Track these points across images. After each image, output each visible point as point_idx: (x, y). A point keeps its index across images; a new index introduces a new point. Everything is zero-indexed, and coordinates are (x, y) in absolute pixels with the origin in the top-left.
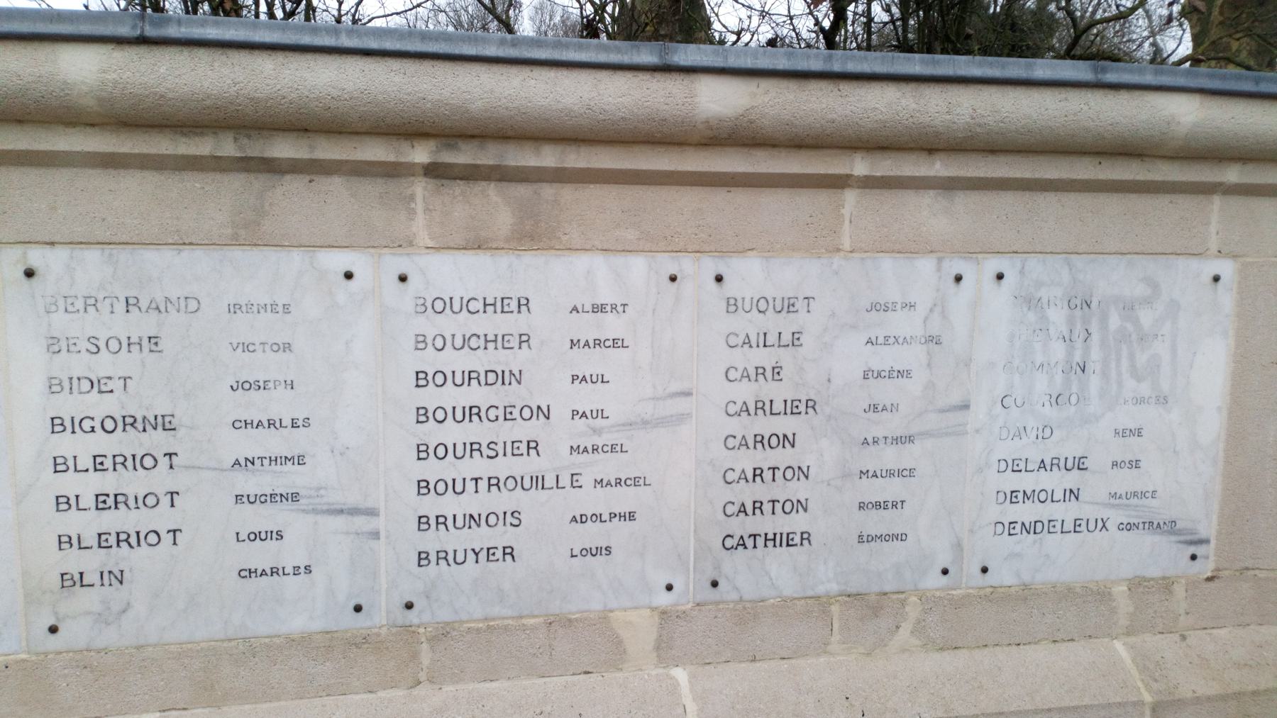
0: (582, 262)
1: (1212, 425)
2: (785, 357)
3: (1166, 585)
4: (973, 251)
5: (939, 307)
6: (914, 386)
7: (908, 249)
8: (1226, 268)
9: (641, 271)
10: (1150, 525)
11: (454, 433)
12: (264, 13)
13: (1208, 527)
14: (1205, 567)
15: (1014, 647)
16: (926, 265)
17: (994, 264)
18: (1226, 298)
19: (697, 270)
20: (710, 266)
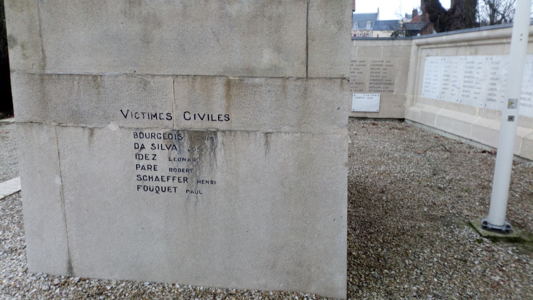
9: (484, 57)
11: (468, 84)
19: (489, 57)
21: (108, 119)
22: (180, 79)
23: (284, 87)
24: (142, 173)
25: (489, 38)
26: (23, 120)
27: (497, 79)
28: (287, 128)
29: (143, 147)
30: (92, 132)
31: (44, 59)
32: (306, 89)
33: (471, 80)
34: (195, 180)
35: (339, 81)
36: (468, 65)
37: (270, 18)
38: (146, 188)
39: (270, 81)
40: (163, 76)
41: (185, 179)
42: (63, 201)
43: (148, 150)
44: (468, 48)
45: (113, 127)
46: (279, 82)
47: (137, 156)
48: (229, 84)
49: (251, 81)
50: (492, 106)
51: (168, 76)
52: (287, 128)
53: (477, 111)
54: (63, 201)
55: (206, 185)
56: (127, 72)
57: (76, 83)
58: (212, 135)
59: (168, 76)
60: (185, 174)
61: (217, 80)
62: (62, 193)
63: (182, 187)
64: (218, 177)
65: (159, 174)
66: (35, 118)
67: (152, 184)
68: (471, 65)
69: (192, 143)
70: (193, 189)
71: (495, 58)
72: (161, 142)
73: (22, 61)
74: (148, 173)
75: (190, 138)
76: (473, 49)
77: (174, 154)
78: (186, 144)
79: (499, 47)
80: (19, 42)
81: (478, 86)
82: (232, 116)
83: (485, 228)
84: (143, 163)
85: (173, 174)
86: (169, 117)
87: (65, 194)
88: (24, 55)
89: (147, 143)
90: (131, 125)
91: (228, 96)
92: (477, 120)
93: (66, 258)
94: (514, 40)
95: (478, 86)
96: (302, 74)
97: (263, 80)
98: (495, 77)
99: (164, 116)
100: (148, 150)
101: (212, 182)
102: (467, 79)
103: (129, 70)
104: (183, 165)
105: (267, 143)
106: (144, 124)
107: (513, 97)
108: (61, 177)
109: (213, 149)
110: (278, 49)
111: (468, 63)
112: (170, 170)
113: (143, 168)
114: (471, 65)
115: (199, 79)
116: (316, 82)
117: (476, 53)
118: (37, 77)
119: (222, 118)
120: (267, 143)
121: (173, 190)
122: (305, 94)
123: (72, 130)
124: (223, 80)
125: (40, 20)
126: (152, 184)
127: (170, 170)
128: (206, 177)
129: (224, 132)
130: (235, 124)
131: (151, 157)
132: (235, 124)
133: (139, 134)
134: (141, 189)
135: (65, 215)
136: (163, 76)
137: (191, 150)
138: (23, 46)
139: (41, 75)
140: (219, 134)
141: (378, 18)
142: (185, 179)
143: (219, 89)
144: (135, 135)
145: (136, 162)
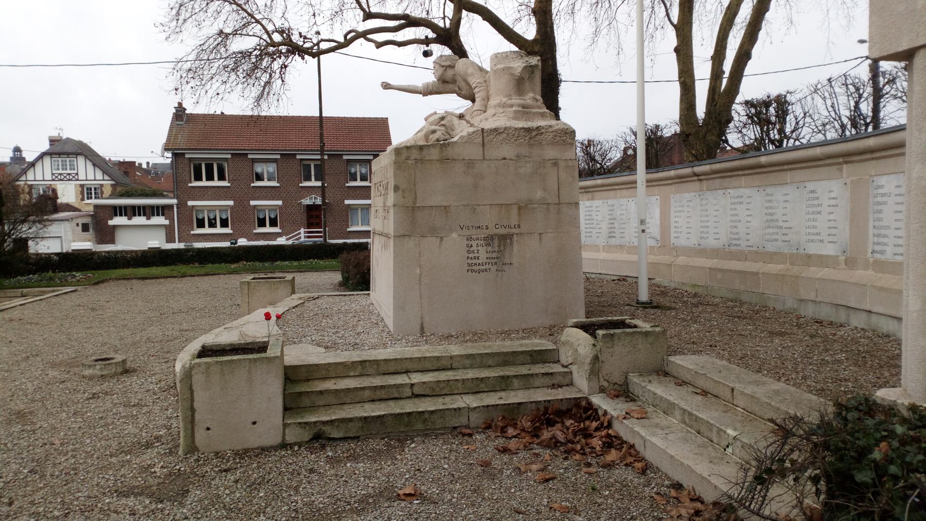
0: (597, 201)
1: (658, 222)
2: (613, 212)
3: (654, 247)
4: (630, 197)
5: (627, 205)
6: (625, 216)
7: (624, 197)
8: (658, 197)
9: (601, 202)
10: (652, 238)
11: (588, 226)
12: (846, 116)
13: (659, 239)
14: (659, 245)
15: (508, 158)
16: (625, 199)
17: (632, 199)
18: (658, 202)
19: (605, 201)
20: (606, 201)
21: (451, 230)
22: (493, 206)
23: (548, 209)
24: (470, 261)
25: (603, 186)
26: (399, 234)
27: (614, 219)
28: (550, 230)
29: (471, 246)
30: (442, 239)
31: (415, 198)
32: (559, 209)
33: (592, 222)
34: (501, 263)
35: (574, 205)
36: (588, 209)
37: (540, 175)
38: (472, 271)
39: (541, 206)
40: (484, 205)
41: (496, 263)
42: (420, 283)
43: (474, 248)
44: (585, 194)
45: (454, 235)
46: (545, 206)
47: (468, 252)
48: (520, 208)
49: (531, 206)
50: (613, 242)
51: (486, 205)
52: (550, 230)
53: (601, 249)
54: (420, 283)
55: (507, 266)
56: (464, 203)
57: (434, 211)
58: (510, 236)
59: (486, 205)
60: (496, 260)
61: (514, 206)
62: (420, 279)
63: (494, 268)
64: (515, 260)
65: (480, 261)
66: (407, 232)
67: (476, 268)
68: (590, 209)
69: (500, 242)
70: (500, 269)
71: (610, 202)
72: (482, 242)
73: (402, 200)
74: (474, 261)
75: (499, 239)
76: (590, 195)
77: (490, 249)
78: (496, 242)
79: (612, 193)
80: (401, 188)
81: (598, 226)
82: (522, 226)
83: (637, 303)
84: (471, 255)
85: (489, 261)
86: (487, 228)
87: (422, 279)
88: (403, 196)
89: (474, 243)
90: (465, 234)
91: (519, 215)
92: (602, 255)
93: (420, 322)
94: (639, 184)
95: (598, 226)
96: (557, 202)
97: (537, 205)
98: (613, 217)
99: (484, 227)
100: (474, 248)
101: (511, 264)
102: (587, 222)
103: (465, 203)
104: (494, 255)
105: (540, 239)
106: (473, 232)
107: (643, 218)
108: (420, 268)
109: (511, 244)
110: (545, 190)
111: (587, 207)
112: (487, 258)
113: (471, 259)
114: (590, 209)
115: (504, 206)
116: (564, 205)
117: (593, 199)
118: (410, 208)
119: (516, 226)
120: (540, 239)
121: (488, 270)
122: (559, 211)
123: (430, 239)
124: (517, 206)
125: (415, 176)
126: (476, 268)
127: (487, 258)
128: (507, 261)
129: (517, 234)
130: (523, 229)
131: (476, 252)
132: (523, 229)
133: (469, 238)
134: (470, 272)
135: (421, 293)
136: (484, 205)
137: (499, 246)
138: (403, 191)
139: (413, 207)
140: (515, 236)
141: (7, 162)
142: (496, 263)
143: (515, 211)
144: (467, 239)
145: (467, 255)
